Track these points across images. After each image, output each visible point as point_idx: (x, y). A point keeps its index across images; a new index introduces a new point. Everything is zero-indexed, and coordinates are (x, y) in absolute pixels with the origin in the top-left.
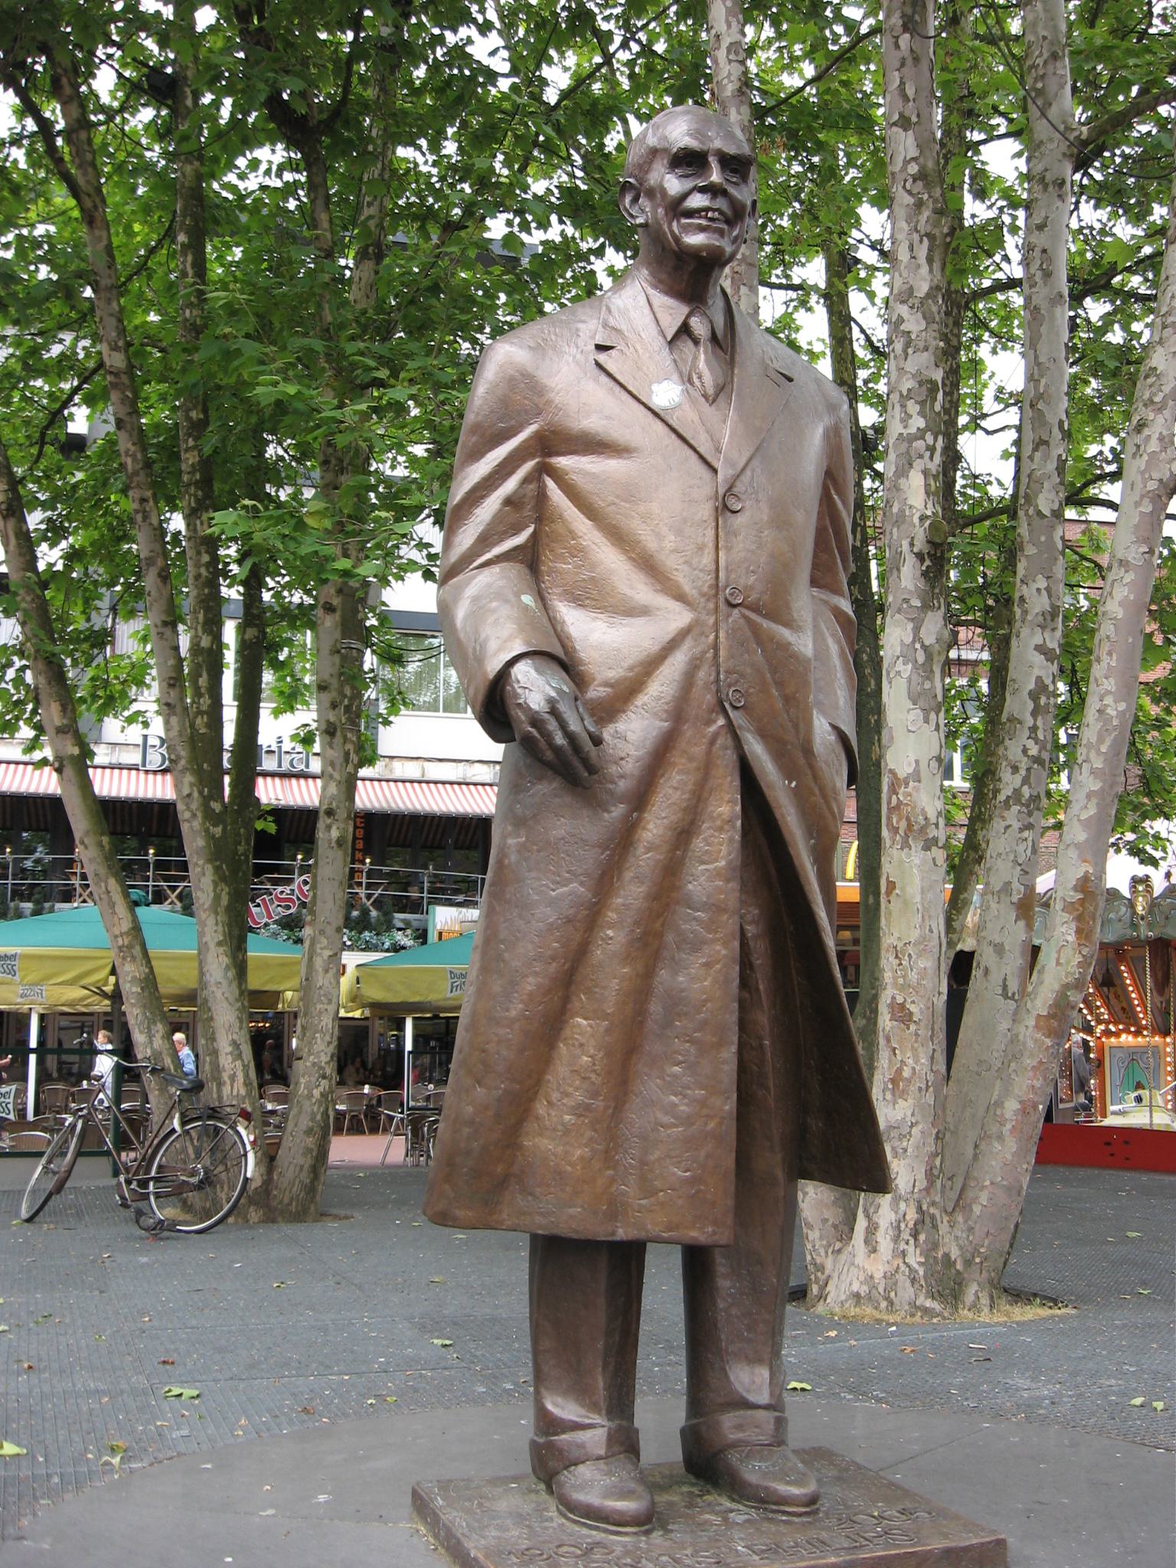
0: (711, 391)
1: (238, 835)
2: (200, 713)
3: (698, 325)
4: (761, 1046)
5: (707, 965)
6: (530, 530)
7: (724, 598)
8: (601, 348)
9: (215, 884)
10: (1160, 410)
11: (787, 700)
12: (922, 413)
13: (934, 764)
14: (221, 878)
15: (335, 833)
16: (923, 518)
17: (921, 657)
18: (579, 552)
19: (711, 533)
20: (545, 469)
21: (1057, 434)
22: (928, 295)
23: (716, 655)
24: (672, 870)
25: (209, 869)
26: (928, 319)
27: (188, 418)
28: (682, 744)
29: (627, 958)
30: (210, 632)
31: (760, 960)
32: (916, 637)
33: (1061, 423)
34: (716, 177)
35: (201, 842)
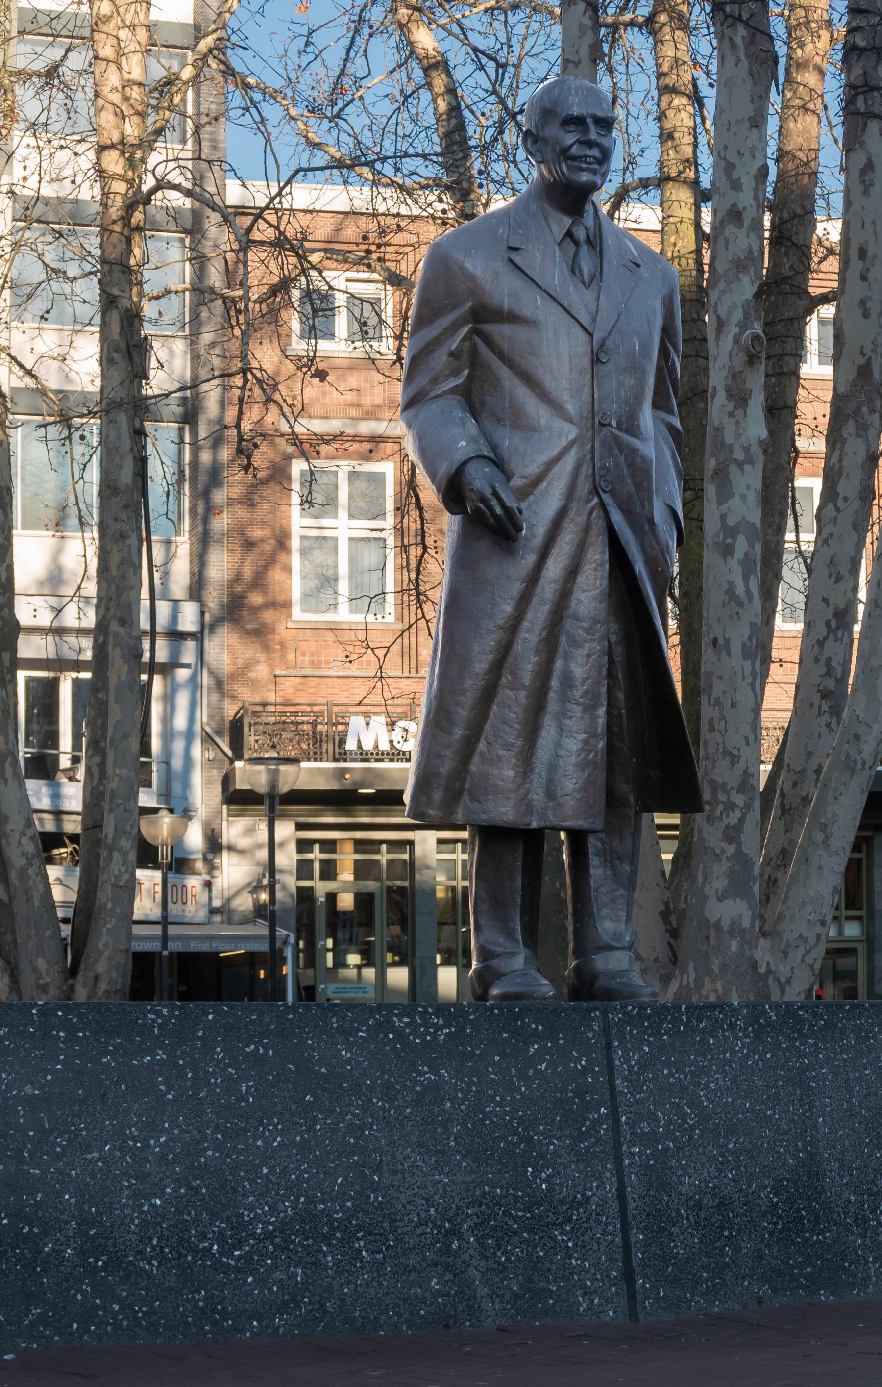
0: (587, 279)
4: (620, 714)
5: (588, 656)
6: (466, 372)
7: (594, 421)
8: (512, 249)
11: (638, 486)
19: (588, 376)
20: (474, 331)
23: (593, 458)
24: (564, 595)
28: (572, 514)
29: (537, 652)
31: (619, 650)
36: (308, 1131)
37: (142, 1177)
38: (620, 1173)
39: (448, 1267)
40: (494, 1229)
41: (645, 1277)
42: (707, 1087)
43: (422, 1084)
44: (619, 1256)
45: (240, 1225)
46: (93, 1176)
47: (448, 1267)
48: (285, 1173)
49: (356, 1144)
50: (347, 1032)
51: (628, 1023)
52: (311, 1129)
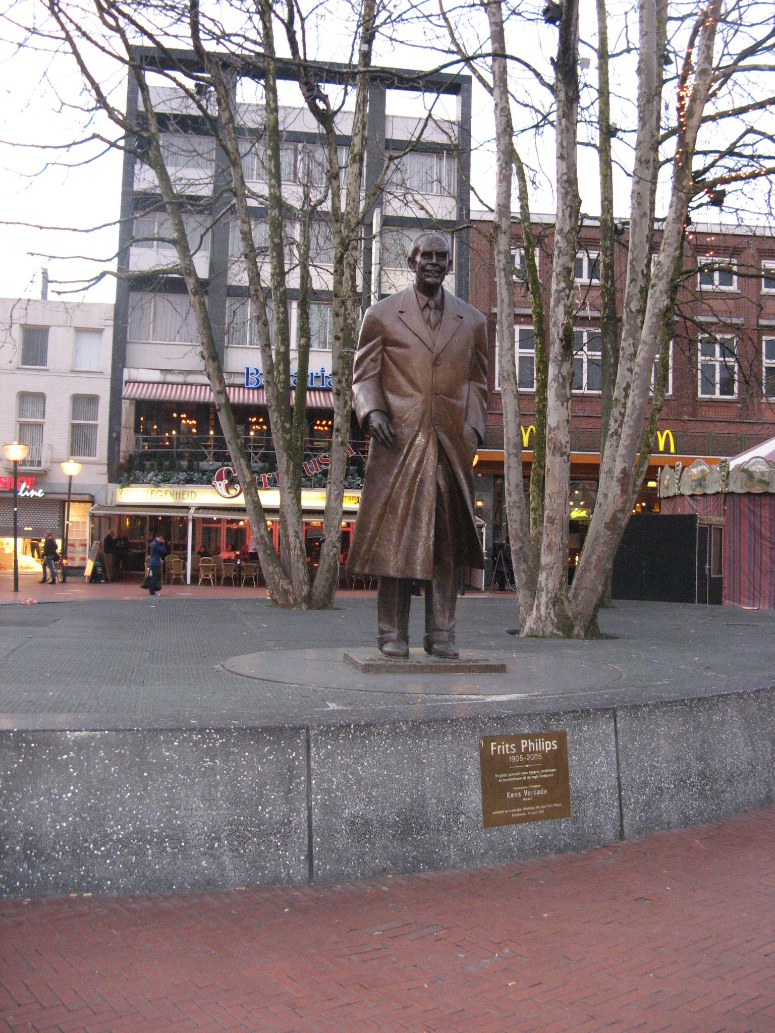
1: (297, 437)
2: (280, 382)
3: (432, 304)
7: (434, 392)
8: (401, 312)
9: (287, 461)
10: (660, 280)
12: (564, 281)
13: (565, 423)
14: (290, 458)
15: (340, 439)
16: (563, 324)
17: (561, 380)
18: (393, 377)
20: (384, 350)
21: (640, 276)
22: (568, 232)
25: (285, 454)
26: (568, 241)
27: (273, 242)
30: (284, 345)
32: (560, 372)
33: (642, 271)
34: (434, 260)
35: (281, 443)
36: (144, 790)
37: (57, 812)
38: (310, 809)
39: (212, 855)
40: (238, 837)
41: (319, 859)
42: (362, 765)
43: (205, 767)
44: (305, 849)
45: (107, 835)
46: (33, 812)
47: (212, 855)
48: (130, 811)
49: (168, 797)
50: (168, 742)
51: (320, 735)
52: (145, 789)
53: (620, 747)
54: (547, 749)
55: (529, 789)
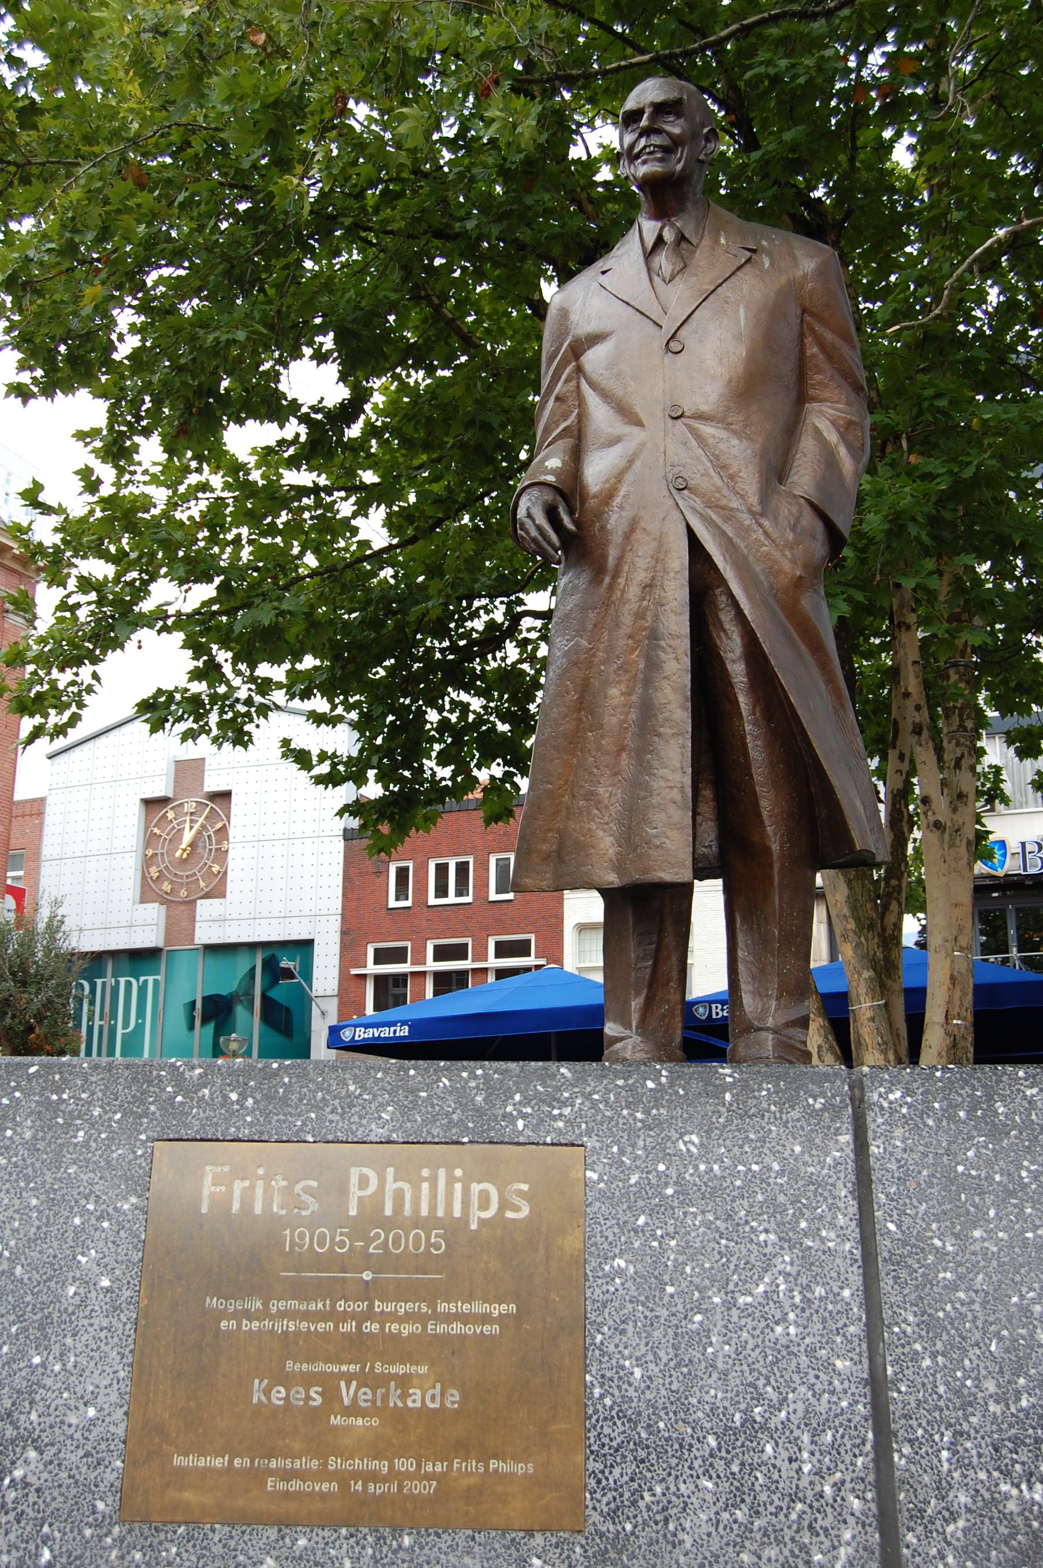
53: (884, 1245)
54: (477, 1215)
55: (364, 1380)
